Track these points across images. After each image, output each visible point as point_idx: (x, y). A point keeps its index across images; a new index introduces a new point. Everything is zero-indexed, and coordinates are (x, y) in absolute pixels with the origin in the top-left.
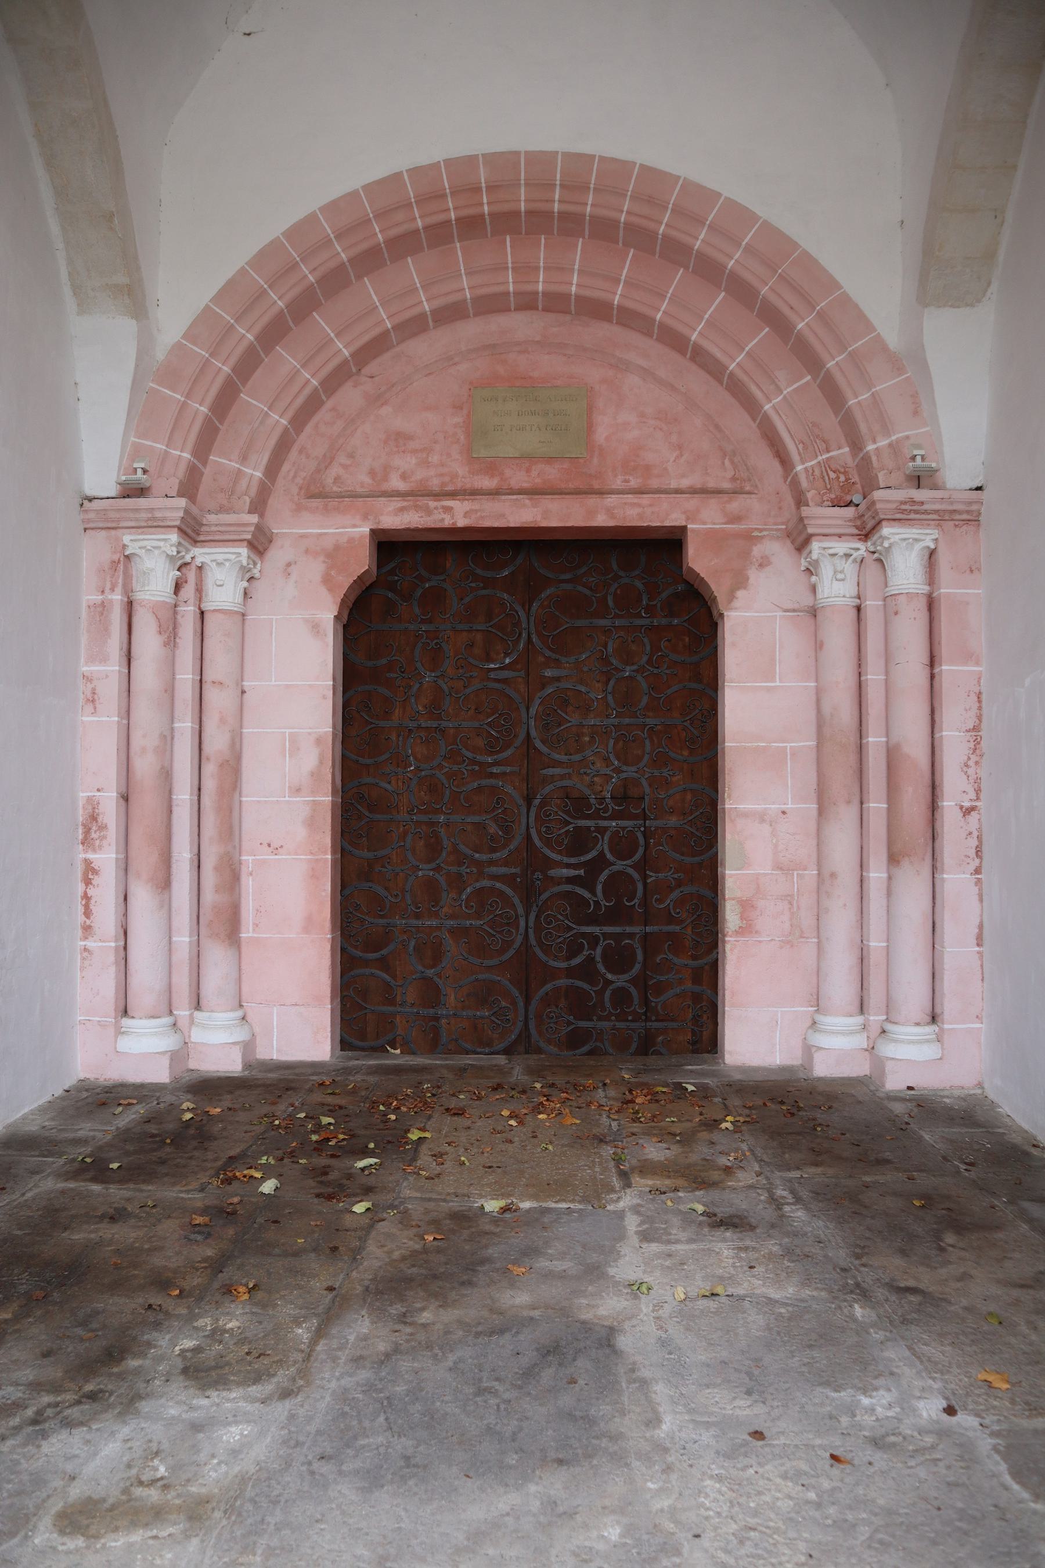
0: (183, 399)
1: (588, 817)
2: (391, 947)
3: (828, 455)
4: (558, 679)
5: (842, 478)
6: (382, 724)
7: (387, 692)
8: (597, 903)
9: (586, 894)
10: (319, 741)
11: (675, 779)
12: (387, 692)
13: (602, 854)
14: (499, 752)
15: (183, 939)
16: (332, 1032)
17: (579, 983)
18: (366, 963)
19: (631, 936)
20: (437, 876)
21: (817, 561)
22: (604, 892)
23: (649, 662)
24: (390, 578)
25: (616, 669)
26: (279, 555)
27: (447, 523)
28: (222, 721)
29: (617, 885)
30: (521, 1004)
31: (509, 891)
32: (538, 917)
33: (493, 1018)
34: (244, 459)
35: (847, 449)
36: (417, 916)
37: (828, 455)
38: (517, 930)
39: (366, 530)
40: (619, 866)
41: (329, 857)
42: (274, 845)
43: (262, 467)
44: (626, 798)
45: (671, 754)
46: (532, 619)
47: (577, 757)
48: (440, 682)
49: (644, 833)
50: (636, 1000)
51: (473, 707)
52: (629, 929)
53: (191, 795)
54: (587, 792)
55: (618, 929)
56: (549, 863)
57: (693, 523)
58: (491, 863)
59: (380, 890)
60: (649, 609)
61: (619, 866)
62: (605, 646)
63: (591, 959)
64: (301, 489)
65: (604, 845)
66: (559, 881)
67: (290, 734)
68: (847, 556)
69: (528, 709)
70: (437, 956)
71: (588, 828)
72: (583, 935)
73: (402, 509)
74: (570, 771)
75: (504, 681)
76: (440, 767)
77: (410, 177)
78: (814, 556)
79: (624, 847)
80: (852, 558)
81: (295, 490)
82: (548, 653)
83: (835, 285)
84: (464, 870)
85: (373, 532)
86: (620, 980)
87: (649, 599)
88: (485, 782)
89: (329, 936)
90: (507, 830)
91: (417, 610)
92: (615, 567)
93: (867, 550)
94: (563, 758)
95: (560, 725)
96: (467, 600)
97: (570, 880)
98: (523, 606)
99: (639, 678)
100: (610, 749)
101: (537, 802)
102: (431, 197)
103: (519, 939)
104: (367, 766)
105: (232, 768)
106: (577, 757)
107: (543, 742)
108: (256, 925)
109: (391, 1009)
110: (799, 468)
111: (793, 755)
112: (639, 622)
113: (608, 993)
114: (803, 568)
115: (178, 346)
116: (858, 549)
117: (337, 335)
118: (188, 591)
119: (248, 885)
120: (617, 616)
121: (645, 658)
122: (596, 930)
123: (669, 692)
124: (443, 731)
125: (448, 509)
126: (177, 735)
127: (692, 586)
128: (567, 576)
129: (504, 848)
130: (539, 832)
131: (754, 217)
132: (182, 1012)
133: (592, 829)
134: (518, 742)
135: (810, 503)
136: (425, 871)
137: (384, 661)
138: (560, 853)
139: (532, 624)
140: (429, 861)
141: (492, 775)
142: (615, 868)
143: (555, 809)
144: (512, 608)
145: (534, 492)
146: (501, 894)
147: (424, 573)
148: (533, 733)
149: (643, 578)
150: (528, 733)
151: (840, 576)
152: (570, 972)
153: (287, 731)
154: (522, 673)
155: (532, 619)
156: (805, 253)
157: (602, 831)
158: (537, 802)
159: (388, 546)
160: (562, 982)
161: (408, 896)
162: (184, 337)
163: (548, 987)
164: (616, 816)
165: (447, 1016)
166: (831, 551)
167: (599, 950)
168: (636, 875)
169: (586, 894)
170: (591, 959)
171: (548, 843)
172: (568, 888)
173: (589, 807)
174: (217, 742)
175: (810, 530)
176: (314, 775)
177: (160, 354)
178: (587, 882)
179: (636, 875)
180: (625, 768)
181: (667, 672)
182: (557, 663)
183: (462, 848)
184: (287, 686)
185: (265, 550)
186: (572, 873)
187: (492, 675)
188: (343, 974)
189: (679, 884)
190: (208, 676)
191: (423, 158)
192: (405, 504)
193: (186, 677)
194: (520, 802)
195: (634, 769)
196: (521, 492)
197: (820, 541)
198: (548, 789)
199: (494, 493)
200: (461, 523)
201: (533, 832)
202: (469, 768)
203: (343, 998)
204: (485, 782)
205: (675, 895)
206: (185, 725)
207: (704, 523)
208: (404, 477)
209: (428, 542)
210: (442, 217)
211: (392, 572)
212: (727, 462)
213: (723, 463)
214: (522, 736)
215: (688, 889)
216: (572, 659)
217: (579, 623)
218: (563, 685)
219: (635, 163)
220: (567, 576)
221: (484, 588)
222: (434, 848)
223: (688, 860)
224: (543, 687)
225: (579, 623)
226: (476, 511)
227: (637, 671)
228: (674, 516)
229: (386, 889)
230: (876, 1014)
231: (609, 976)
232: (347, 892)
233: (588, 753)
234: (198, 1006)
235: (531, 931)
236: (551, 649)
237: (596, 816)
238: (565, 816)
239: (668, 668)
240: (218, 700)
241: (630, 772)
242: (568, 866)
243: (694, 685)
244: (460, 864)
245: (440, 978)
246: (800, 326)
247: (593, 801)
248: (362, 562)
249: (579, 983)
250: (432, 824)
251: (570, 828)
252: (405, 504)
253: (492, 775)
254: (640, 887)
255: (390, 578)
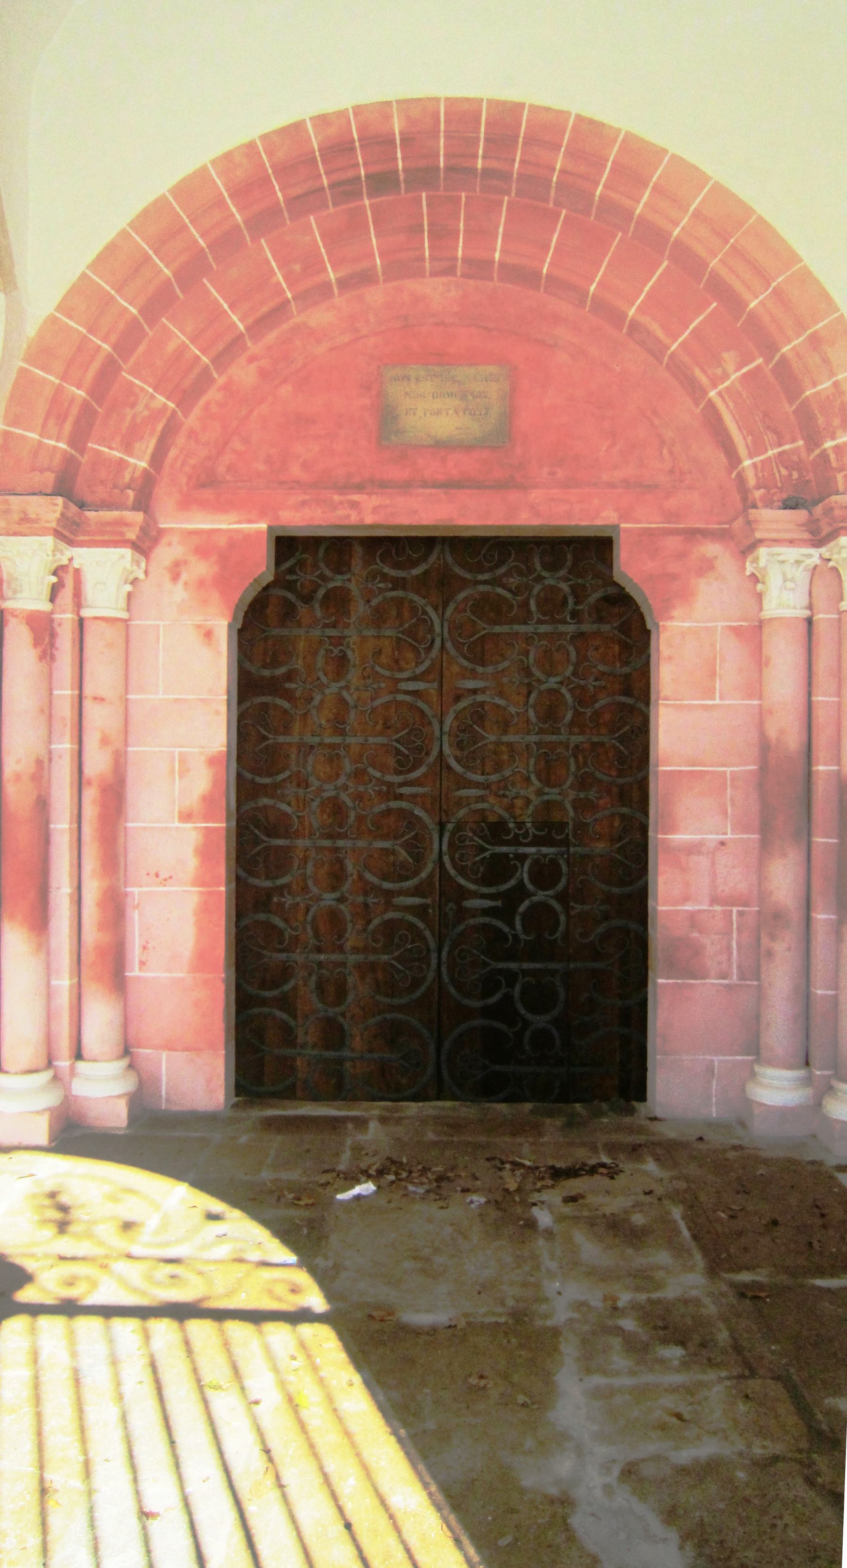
0: (57, 381)
1: (507, 843)
2: (292, 983)
3: (780, 449)
4: (475, 692)
5: (795, 475)
6: (281, 739)
7: (286, 705)
8: (516, 937)
9: (506, 929)
10: (212, 761)
11: (601, 802)
12: (286, 705)
13: (521, 881)
14: (409, 771)
15: (64, 983)
16: (226, 1079)
17: (495, 1024)
18: (263, 1002)
19: (553, 973)
20: (342, 907)
21: (765, 568)
22: (523, 926)
23: (574, 674)
24: (288, 577)
25: (539, 681)
26: (166, 553)
27: (354, 518)
28: (105, 741)
29: (540, 916)
30: (432, 1048)
31: (421, 925)
32: (450, 952)
33: (401, 1061)
34: (128, 448)
35: (801, 443)
36: (319, 950)
37: (780, 449)
38: (429, 965)
39: (263, 526)
40: (540, 896)
41: (223, 889)
42: (163, 875)
43: (148, 457)
44: (549, 830)
45: (598, 775)
46: (446, 625)
47: (494, 778)
48: (345, 694)
49: (568, 862)
50: (558, 1042)
51: (381, 722)
52: (552, 966)
53: (71, 823)
54: (506, 815)
55: (538, 966)
56: (463, 894)
57: (627, 522)
58: (401, 893)
59: (277, 921)
60: (575, 614)
61: (540, 896)
62: (527, 653)
63: (508, 999)
64: (190, 478)
65: (524, 873)
66: (474, 913)
67: (180, 753)
68: (798, 562)
69: (441, 723)
70: (341, 992)
71: (506, 855)
72: (500, 971)
73: (304, 503)
74: (487, 792)
75: (415, 693)
76: (345, 788)
77: (314, 126)
78: (762, 563)
79: (545, 874)
80: (803, 565)
81: (184, 480)
82: (465, 663)
83: (794, 258)
84: (371, 900)
85: (270, 528)
86: (540, 1021)
87: (576, 603)
88: (394, 804)
89: (223, 975)
90: (419, 859)
91: (319, 613)
92: (538, 566)
93: (821, 557)
94: (479, 778)
95: (475, 743)
96: (375, 602)
97: (486, 912)
98: (436, 609)
99: (564, 690)
100: (531, 769)
101: (450, 826)
102: (338, 149)
103: (431, 975)
104: (265, 786)
105: (115, 796)
106: (494, 778)
107: (458, 760)
108: (142, 963)
109: (293, 1051)
110: (747, 463)
111: (733, 779)
112: (562, 628)
113: (528, 1034)
114: (748, 573)
115: (52, 320)
116: (811, 556)
117: (231, 307)
118: (67, 593)
119: (136, 921)
120: (540, 622)
121: (571, 668)
122: (513, 966)
123: (597, 706)
124: (347, 747)
125: (354, 505)
126: (55, 758)
127: (623, 589)
128: (486, 576)
129: (414, 877)
130: (452, 860)
131: (703, 178)
132: (63, 1063)
133: (511, 856)
134: (432, 758)
135: (759, 504)
136: (329, 899)
137: (283, 670)
138: (475, 882)
139: (446, 630)
140: (334, 889)
141: (400, 797)
142: (535, 899)
143: (471, 834)
144: (425, 613)
145: (450, 485)
146: (411, 926)
147: (328, 573)
148: (447, 750)
149: (569, 580)
150: (441, 751)
151: (789, 585)
152: (486, 1012)
153: (177, 750)
154: (435, 685)
155: (446, 625)
156: (761, 219)
157: (522, 858)
158: (450, 826)
159: (286, 546)
160: (477, 1022)
161: (309, 927)
162: (59, 308)
163: (463, 1027)
164: (537, 842)
165: (352, 1060)
166: (781, 558)
167: (517, 989)
168: (557, 907)
169: (506, 929)
170: (508, 999)
171: (462, 871)
172: (487, 920)
173: (508, 831)
174: (97, 763)
175: (758, 535)
176: (207, 800)
177: (31, 330)
178: (506, 913)
179: (557, 907)
180: (547, 790)
181: (594, 683)
182: (474, 675)
183: (369, 876)
184: (176, 700)
185: (151, 549)
186: (487, 903)
187: (403, 686)
188: (238, 1012)
189: (606, 917)
190: (88, 691)
191: (329, 106)
192: (307, 497)
193: (65, 692)
194: (432, 826)
195: (556, 790)
196: (436, 485)
197: (768, 546)
198: (462, 813)
199: (406, 486)
200: (369, 520)
201: (446, 859)
202: (377, 788)
203: (238, 1046)
204: (394, 804)
205: (601, 929)
206: (64, 746)
207: (639, 522)
208: (305, 466)
209: (331, 538)
210: (350, 174)
211: (291, 571)
212: (665, 451)
213: (661, 453)
214: (435, 753)
215: (616, 922)
216: (490, 669)
217: (497, 629)
218: (480, 698)
219: (569, 113)
220: (486, 576)
221: (393, 589)
222: (337, 877)
223: (616, 890)
224: (458, 698)
225: (497, 629)
226: (386, 506)
227: (561, 683)
228: (604, 514)
229: (286, 920)
230: (820, 1069)
231: (529, 1016)
232: (245, 922)
233: (507, 773)
234: (78, 1055)
235: (444, 969)
236: (466, 658)
237: (516, 842)
238: (480, 842)
239: (596, 679)
240: (99, 718)
241: (553, 794)
242: (483, 896)
243: (623, 699)
244: (366, 893)
245: (344, 1017)
246: (752, 305)
247: (511, 825)
248: (260, 565)
249: (495, 1024)
250: (337, 850)
251: (487, 854)
252: (307, 497)
253: (400, 797)
254: (563, 918)
255: (288, 577)
